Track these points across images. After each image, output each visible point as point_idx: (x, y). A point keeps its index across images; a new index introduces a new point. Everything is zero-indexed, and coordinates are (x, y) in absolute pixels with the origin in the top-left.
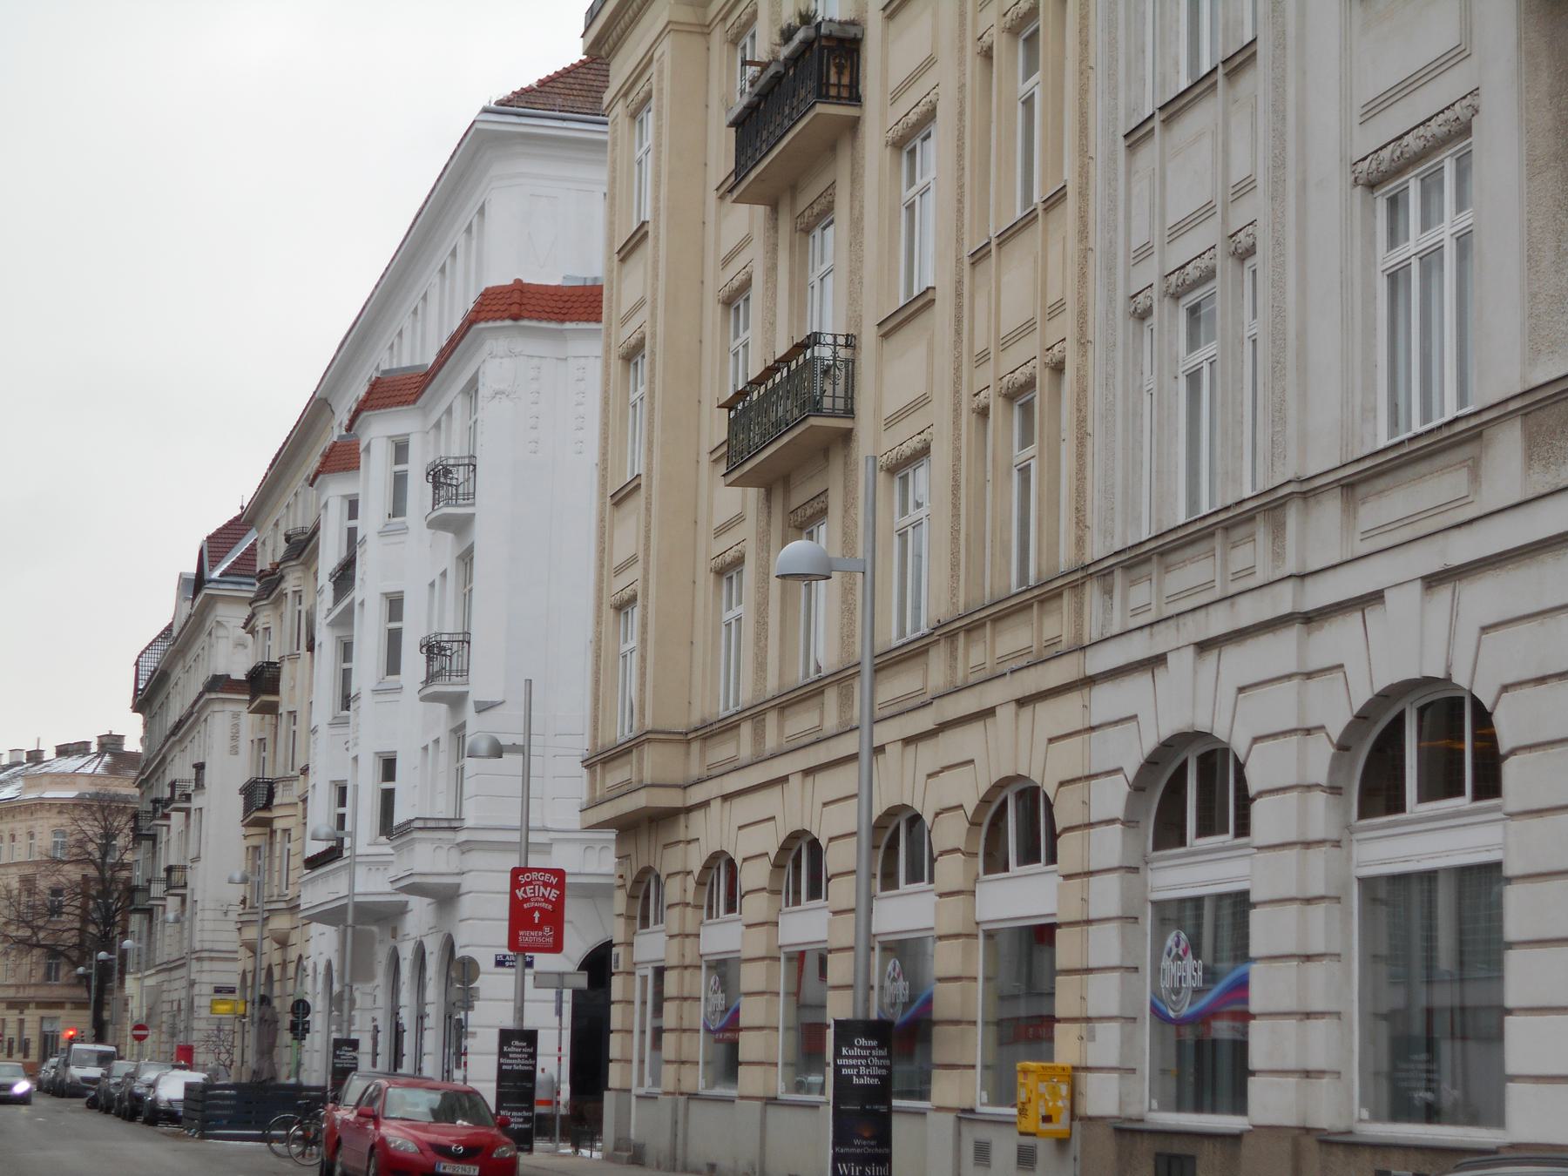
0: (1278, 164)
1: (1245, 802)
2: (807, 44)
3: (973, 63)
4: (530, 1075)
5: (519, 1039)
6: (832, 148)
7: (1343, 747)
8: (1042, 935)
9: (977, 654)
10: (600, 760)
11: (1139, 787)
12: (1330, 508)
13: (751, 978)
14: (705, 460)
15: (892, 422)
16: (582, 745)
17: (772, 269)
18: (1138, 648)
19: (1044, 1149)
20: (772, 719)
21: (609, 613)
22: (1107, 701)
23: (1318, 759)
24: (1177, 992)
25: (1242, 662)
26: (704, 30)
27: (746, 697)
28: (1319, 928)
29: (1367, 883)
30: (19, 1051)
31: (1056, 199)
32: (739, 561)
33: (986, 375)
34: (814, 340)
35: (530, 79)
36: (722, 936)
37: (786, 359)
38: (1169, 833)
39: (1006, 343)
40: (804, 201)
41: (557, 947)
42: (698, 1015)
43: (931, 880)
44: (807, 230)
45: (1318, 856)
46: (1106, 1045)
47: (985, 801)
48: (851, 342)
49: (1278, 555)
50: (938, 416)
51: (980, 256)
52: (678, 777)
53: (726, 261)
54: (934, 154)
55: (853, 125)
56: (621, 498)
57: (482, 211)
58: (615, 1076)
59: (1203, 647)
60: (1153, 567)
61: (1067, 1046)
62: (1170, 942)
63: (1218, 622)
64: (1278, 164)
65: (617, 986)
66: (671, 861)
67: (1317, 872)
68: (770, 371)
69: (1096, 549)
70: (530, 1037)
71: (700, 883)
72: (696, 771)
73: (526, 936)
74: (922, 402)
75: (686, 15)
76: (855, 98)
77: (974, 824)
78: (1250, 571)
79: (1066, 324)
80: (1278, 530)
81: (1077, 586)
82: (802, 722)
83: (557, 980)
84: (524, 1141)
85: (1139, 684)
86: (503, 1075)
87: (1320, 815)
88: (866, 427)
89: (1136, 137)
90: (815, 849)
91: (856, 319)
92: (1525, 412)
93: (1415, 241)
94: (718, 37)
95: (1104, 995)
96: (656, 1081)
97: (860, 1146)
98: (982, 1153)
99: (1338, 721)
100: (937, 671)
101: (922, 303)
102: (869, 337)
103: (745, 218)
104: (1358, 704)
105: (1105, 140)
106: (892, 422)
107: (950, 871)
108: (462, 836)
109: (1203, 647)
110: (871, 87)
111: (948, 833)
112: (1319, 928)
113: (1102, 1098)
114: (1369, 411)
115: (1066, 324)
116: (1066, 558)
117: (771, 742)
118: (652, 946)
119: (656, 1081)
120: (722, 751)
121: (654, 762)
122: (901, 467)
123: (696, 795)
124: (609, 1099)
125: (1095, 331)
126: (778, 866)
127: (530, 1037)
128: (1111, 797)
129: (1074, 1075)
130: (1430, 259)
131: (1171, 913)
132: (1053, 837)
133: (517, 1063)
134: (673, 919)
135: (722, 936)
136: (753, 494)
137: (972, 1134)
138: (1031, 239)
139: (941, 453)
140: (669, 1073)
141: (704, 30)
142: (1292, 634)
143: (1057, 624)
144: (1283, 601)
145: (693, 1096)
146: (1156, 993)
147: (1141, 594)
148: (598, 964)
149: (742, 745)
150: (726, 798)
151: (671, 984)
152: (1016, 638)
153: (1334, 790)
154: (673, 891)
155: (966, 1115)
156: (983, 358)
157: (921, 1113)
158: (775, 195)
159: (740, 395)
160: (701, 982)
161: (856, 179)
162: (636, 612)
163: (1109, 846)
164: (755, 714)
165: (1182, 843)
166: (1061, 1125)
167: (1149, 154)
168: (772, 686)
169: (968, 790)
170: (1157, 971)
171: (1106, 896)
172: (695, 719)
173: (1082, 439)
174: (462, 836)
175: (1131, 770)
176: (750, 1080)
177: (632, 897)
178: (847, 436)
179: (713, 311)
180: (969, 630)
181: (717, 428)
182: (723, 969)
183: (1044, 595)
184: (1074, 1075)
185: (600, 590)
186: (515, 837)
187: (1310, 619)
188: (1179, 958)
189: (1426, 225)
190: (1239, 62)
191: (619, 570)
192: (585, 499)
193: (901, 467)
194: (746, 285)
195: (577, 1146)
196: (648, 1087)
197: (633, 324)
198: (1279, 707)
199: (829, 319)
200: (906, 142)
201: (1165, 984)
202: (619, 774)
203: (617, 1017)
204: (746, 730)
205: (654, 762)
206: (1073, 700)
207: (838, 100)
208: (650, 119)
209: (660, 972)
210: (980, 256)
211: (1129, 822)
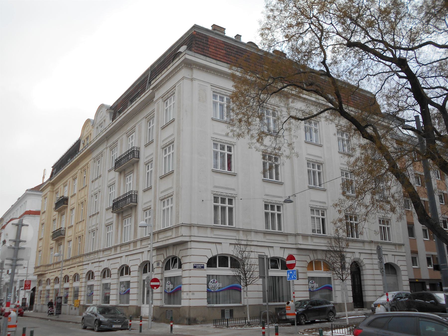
0: (100, 223)
1: (130, 272)
2: (63, 199)
3: (78, 205)
4: (25, 303)
5: (24, 299)
6: (65, 208)
7: (102, 273)
8: (78, 288)
9: (74, 261)
10: (36, 268)
11: (87, 275)
12: (102, 252)
13: (51, 292)
14: (50, 237)
15: (69, 237)
16: (34, 266)
17: (58, 218)
18: (87, 263)
19: (77, 307)
20: (55, 265)
21: (38, 252)
22: (85, 267)
23: (100, 273)
24: (169, 289)
25: (111, 262)
26: (53, 191)
27: (53, 262)
28: (99, 288)
29: (103, 284)
30: (16, 282)
31: (84, 220)
32: (53, 248)
33: (77, 235)
34: (61, 228)
35: (33, 187)
36: (48, 287)
37: (59, 229)
38: (122, 274)
39: (79, 232)
40: (62, 213)
41: (29, 289)
42: (45, 296)
43: (110, 277)
44: (62, 215)
45: (99, 282)
46: (82, 298)
47: (74, 275)
48: (65, 228)
49: (98, 256)
50: (73, 237)
51: (77, 223)
52: (45, 270)
53: (54, 216)
54: (74, 211)
55: (67, 207)
56: (40, 239)
57: (26, 201)
58: (35, 303)
59: (92, 263)
60: (94, 254)
61: (79, 298)
62: (168, 282)
63: (93, 261)
64: (100, 223)
65: (36, 293)
66: (43, 279)
67: (99, 283)
68: (57, 230)
69: (85, 253)
70: (26, 299)
71: (46, 282)
72: (46, 270)
73: (26, 288)
74: (71, 236)
75: (51, 190)
76: (67, 204)
77: (73, 277)
78: (96, 257)
79: (83, 232)
80: (98, 254)
81: (83, 256)
82: (58, 266)
83: (29, 292)
84: (25, 310)
85: (87, 266)
86: (22, 303)
87: (99, 278)
88: (66, 237)
89: (90, 217)
90: (93, 273)
91: (66, 226)
92: (114, 247)
93: (166, 207)
94: (54, 193)
95: (82, 293)
96: (40, 303)
97: (58, 308)
98: (72, 309)
99: (101, 270)
100: (70, 262)
101: (72, 226)
102: (67, 228)
103: (55, 213)
104: (141, 262)
105: (88, 216)
106: (69, 237)
107: (71, 282)
108: (18, 275)
109: (78, 266)
110: (69, 204)
111: (71, 278)
112: (99, 288)
113: (82, 303)
114: (105, 245)
115: (83, 232)
116: (82, 253)
117: (55, 267)
118: (40, 288)
119: (40, 303)
120: (50, 268)
121: (42, 269)
122: (69, 241)
123: (46, 272)
124: (34, 305)
125: (86, 233)
126: (55, 280)
127: (26, 299)
128: (84, 276)
129: (80, 301)
130: (168, 209)
131: (122, 283)
132: (111, 275)
133: (24, 302)
134: (43, 286)
135: (48, 287)
136: (55, 241)
137: (71, 307)
138: (81, 223)
139: (73, 240)
140: (41, 302)
141: (53, 191)
142: (98, 263)
143: (81, 259)
144: (97, 260)
145: (44, 304)
146: (120, 291)
147: (88, 258)
148: (34, 289)
149: (52, 267)
150: (50, 273)
151: (42, 292)
152: (78, 260)
153: (101, 276)
154: (43, 282)
155: (71, 305)
156: (77, 233)
157: (66, 305)
158: (59, 211)
159: (54, 232)
160: (45, 292)
161: (67, 212)
162: (41, 252)
163: (84, 280)
164: (53, 264)
165: (123, 276)
166: (78, 305)
167: (91, 219)
168: (55, 261)
169: (73, 274)
170: (165, 286)
171: (83, 284)
172: (47, 264)
173: (84, 243)
174: (18, 275)
175: (86, 273)
176: (69, 303)
177: (38, 283)
178: (64, 238)
179: (52, 221)
180: (87, 255)
181: (51, 234)
182: (48, 290)
183: (80, 256)
184: (80, 301)
185: (37, 250)
186: (26, 275)
187: (100, 262)
188: (169, 284)
189: (167, 205)
190: (98, 213)
191: (40, 247)
192: (36, 239)
193: (69, 241)
194: (56, 219)
195: (30, 311)
196: (39, 304)
197: (43, 221)
198: (97, 269)
199: (63, 226)
200: (72, 210)
201: (167, 288)
202: (38, 270)
203: (36, 296)
204: (52, 266)
205: (42, 269)
206: (82, 266)
207: (66, 204)
208: (47, 199)
209: (41, 291)
210: (77, 223)
211: (86, 278)
